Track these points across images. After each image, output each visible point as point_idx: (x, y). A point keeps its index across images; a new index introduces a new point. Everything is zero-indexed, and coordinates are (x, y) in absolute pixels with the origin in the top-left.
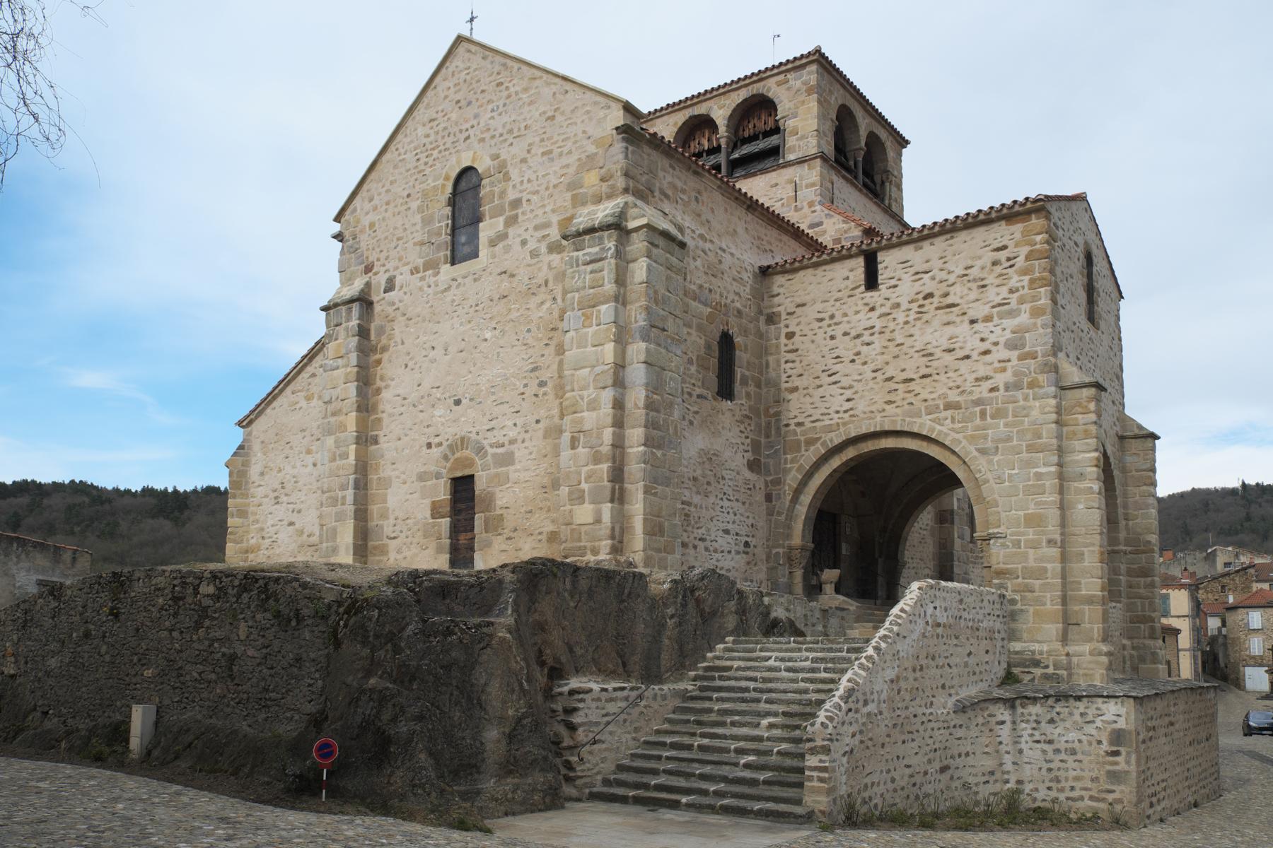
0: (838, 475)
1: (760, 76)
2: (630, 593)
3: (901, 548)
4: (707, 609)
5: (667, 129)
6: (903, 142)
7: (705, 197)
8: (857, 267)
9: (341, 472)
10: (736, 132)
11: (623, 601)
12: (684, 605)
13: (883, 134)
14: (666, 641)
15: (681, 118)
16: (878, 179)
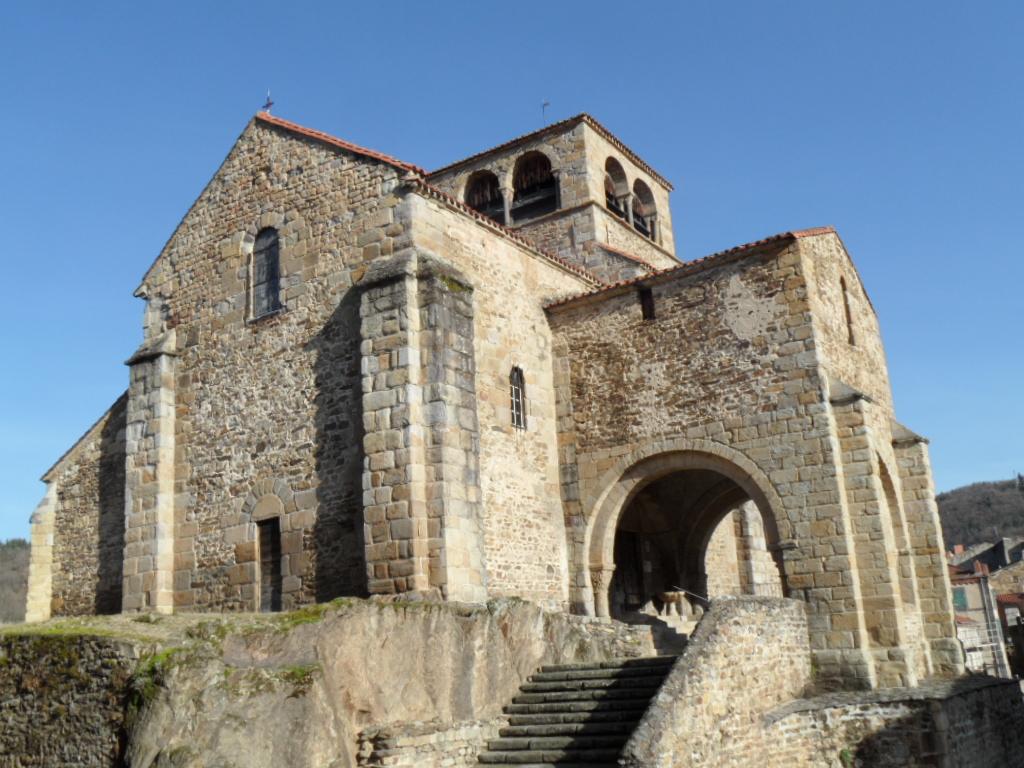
1: (536, 137)
2: (436, 628)
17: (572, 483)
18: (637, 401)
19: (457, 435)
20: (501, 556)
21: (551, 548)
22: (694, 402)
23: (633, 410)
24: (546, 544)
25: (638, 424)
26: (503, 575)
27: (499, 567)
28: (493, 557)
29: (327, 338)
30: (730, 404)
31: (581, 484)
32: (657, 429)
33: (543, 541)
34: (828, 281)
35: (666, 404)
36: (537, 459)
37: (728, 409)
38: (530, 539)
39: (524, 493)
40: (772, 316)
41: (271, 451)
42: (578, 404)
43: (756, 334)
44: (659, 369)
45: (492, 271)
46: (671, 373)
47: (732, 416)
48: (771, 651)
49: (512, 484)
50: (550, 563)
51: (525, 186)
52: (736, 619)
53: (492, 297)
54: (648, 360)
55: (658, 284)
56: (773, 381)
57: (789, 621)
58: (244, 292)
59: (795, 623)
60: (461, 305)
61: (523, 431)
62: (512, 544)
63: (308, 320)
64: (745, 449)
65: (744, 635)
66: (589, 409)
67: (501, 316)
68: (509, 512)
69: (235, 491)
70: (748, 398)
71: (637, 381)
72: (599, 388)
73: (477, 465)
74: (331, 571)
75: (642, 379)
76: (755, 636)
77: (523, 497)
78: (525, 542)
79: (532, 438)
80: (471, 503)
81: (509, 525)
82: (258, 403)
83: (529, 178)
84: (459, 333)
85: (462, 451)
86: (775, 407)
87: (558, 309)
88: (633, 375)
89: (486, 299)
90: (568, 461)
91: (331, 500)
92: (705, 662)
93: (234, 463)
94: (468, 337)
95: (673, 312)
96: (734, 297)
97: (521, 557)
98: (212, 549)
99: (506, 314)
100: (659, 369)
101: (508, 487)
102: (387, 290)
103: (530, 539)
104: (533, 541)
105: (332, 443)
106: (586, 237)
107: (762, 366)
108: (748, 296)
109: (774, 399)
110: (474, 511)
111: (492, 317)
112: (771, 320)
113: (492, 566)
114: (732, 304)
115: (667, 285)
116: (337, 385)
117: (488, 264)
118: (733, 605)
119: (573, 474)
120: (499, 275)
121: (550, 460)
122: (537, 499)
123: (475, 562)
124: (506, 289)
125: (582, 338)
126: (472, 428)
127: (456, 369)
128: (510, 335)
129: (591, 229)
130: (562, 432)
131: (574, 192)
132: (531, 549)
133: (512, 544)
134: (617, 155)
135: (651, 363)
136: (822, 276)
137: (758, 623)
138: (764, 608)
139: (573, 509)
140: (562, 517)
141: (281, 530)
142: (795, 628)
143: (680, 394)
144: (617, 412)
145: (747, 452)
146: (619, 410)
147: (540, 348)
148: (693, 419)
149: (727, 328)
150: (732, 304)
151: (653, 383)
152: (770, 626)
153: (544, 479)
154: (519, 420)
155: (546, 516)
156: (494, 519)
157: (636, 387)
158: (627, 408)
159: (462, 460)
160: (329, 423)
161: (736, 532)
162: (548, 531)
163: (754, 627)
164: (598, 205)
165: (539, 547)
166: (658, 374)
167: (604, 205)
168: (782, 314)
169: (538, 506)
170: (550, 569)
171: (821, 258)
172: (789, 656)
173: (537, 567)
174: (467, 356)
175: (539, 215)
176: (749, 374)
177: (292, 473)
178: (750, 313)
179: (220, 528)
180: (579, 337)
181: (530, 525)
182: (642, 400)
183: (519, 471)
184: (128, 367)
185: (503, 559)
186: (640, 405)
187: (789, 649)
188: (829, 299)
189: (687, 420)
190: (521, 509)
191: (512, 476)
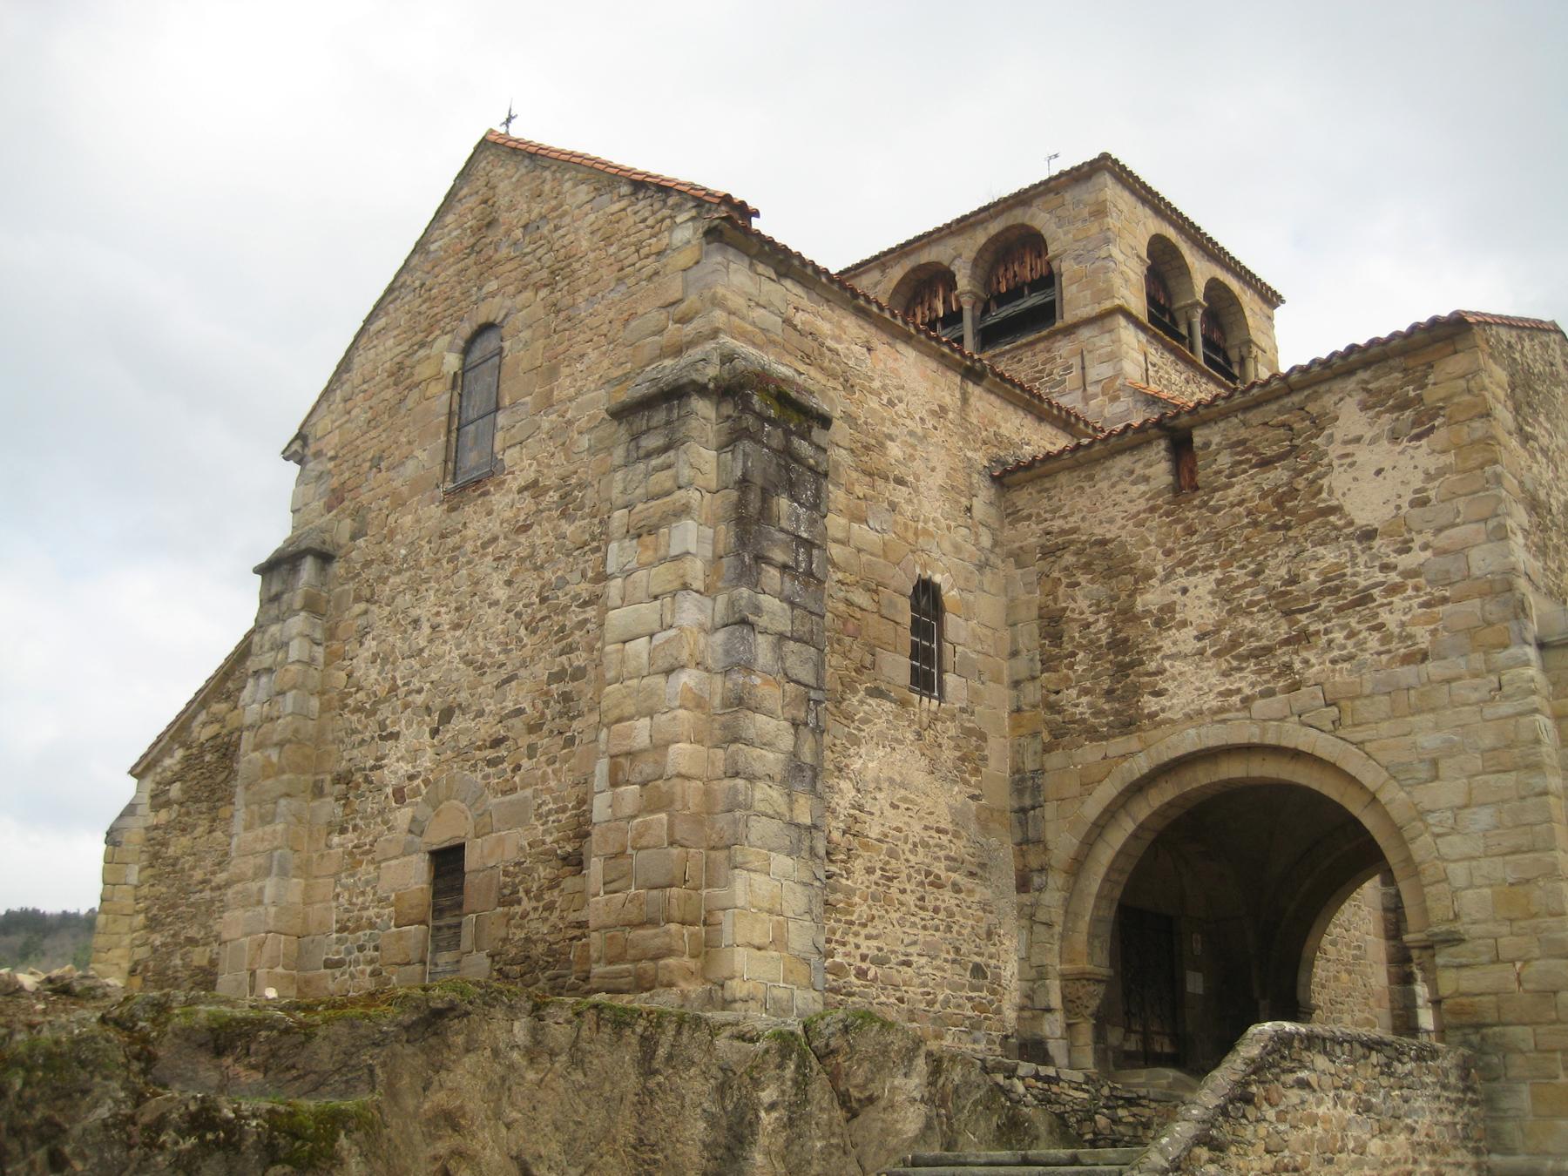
0: (1149, 837)
1: (1022, 199)
2: (670, 1057)
3: (1302, 978)
4: (855, 1093)
5: (880, 287)
6: (1271, 299)
7: (732, 266)
8: (1157, 466)
9: (260, 847)
10: (987, 285)
11: (656, 1072)
12: (801, 1083)
13: (1234, 285)
14: (759, 1158)
15: (897, 273)
16: (1234, 355)
17: (1033, 808)
18: (1159, 649)
19: (778, 693)
20: (868, 937)
21: (982, 932)
22: (1268, 650)
23: (1152, 666)
24: (970, 922)
25: (1158, 694)
26: (871, 975)
27: (864, 958)
28: (851, 939)
29: (564, 515)
30: (1336, 653)
31: (1050, 810)
32: (1196, 700)
33: (966, 917)
34: (1542, 418)
35: (1216, 654)
36: (963, 759)
37: (1334, 662)
38: (936, 910)
39: (931, 821)
40: (1422, 476)
41: (459, 722)
42: (1052, 658)
43: (1389, 511)
44: (1203, 585)
45: (885, 398)
46: (1225, 593)
47: (1342, 676)
48: (1388, 1149)
49: (905, 799)
50: (977, 959)
51: (1003, 289)
52: (1303, 1074)
53: (882, 445)
54: (1180, 570)
55: (1205, 423)
56: (1422, 605)
57: (1438, 1090)
58: (443, 439)
59: (1453, 1095)
60: (803, 447)
61: (935, 702)
62: (895, 916)
63: (535, 483)
64: (1362, 742)
65: (1321, 1111)
66: (1071, 666)
67: (900, 481)
68: (892, 854)
69: (400, 795)
70: (1373, 641)
71: (1161, 610)
72: (1088, 626)
73: (818, 754)
74: (541, 948)
75: (1169, 608)
76: (1350, 1113)
77: (926, 828)
78: (922, 914)
79: (953, 718)
80: (798, 825)
81: (890, 879)
82: (448, 636)
83: (1010, 275)
84: (793, 498)
85: (787, 724)
86: (1424, 656)
87: (1021, 475)
88: (1151, 598)
89: (867, 448)
90: (1030, 765)
91: (549, 812)
92: (1211, 1161)
93: (402, 744)
94: (815, 507)
95: (1232, 475)
96: (1346, 443)
97: (915, 943)
98: (361, 899)
99: (911, 479)
100: (1203, 585)
101: (894, 806)
102: (660, 416)
103: (936, 910)
104: (942, 915)
105: (558, 707)
106: (1106, 371)
107: (1401, 574)
108: (1373, 441)
109: (1424, 640)
110: (807, 843)
111: (879, 483)
112: (1419, 485)
113: (847, 955)
114: (1346, 455)
115: (1222, 425)
116: (574, 598)
117: (876, 384)
118: (1296, 1043)
119: (1037, 789)
120: (900, 407)
121: (992, 763)
122: (956, 835)
123: (801, 937)
124: (912, 433)
125: (1063, 532)
126: (811, 681)
127: (784, 567)
128: (915, 519)
129: (1114, 357)
130: (1019, 710)
131: (1088, 293)
132: (937, 930)
133: (895, 916)
134: (1171, 233)
135: (1187, 574)
136: (1529, 405)
137: (1359, 1088)
138: (1374, 1058)
139: (1034, 862)
140: (1013, 875)
141: (466, 869)
142: (1452, 1107)
143: (1240, 633)
144: (1122, 670)
145: (1368, 747)
146: (1124, 660)
147: (981, 549)
148: (1267, 682)
149: (1334, 503)
150: (1346, 455)
151: (1191, 616)
152: (1387, 1095)
153: (973, 797)
154: (925, 679)
155: (975, 869)
156: (858, 865)
157: (1159, 623)
158: (1142, 663)
159: (787, 741)
160: (556, 669)
161: (1386, 931)
162: (977, 898)
163: (1350, 1096)
164: (1129, 316)
165: (955, 928)
166: (1198, 600)
167: (1144, 318)
168: (1441, 472)
169: (959, 848)
170: (978, 971)
171: (1528, 371)
172: (1432, 1164)
173: (947, 966)
174: (809, 544)
175: (1022, 335)
176: (1376, 592)
177: (491, 763)
178: (1379, 472)
179: (372, 861)
180: (1056, 529)
181: (938, 884)
182: (1168, 647)
183: (919, 778)
184: (259, 577)
185: (874, 943)
186: (1165, 657)
187: (1433, 1149)
188: (1544, 452)
189: (1253, 685)
190: (920, 849)
191: (903, 786)
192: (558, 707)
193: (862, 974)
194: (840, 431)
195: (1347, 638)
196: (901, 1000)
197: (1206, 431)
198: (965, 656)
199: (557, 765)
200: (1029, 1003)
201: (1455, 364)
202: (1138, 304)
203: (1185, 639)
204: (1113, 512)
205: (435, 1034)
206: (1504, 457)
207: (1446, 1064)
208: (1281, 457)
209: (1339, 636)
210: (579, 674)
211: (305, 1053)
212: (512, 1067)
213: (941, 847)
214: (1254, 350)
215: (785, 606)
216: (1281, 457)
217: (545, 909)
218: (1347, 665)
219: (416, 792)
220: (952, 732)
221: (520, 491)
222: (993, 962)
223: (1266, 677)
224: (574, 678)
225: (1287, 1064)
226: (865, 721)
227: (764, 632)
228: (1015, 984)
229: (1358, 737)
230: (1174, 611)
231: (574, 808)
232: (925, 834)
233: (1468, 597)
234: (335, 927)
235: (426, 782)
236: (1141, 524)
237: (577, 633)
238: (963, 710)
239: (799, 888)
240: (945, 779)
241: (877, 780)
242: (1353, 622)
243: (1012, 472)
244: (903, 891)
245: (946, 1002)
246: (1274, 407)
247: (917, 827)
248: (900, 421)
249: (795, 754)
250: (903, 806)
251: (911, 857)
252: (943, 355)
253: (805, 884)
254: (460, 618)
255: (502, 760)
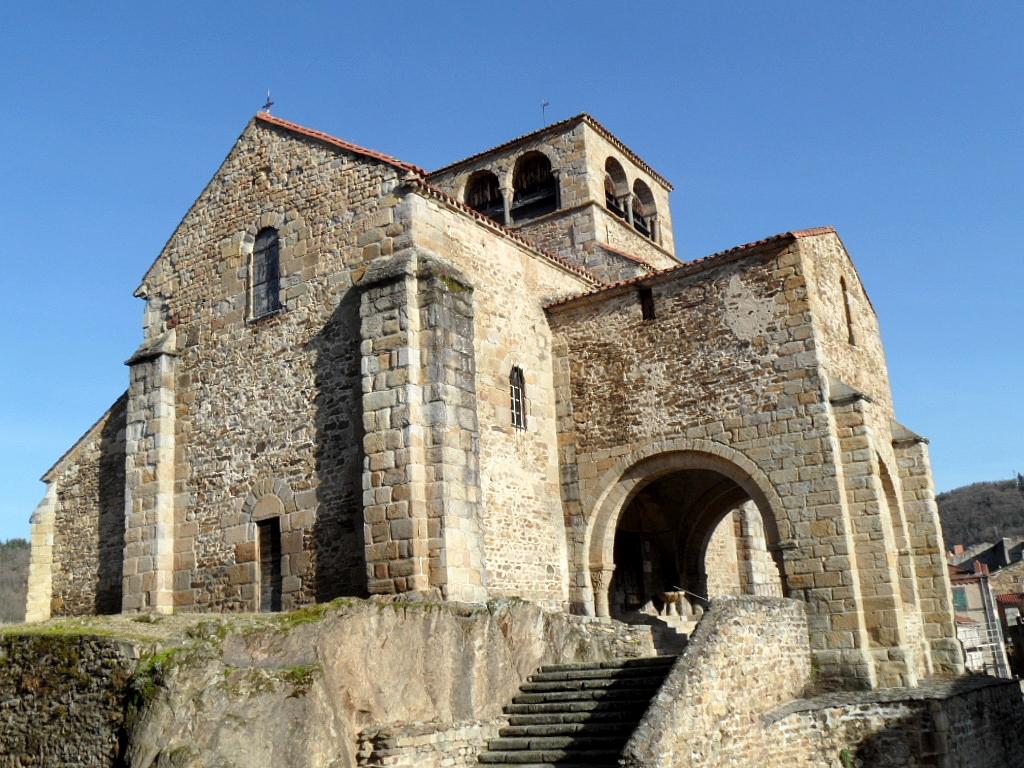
1: (536, 137)
17: (572, 483)
18: (637, 401)
20: (501, 556)
25: (638, 424)
26: (503, 576)
27: (499, 567)
28: (493, 557)
29: (327, 338)
32: (657, 429)
34: (828, 282)
36: (537, 459)
37: (728, 409)
38: (530, 539)
41: (271, 451)
44: (659, 369)
45: (492, 271)
46: (671, 373)
47: (732, 417)
50: (550, 563)
52: (736, 619)
53: (492, 297)
55: (658, 284)
59: (795, 623)
60: (461, 305)
61: (523, 431)
62: (512, 544)
66: (590, 409)
67: (501, 316)
68: (509, 512)
70: (748, 398)
73: (477, 464)
74: (331, 571)
76: (755, 635)
80: (471, 503)
81: (508, 525)
83: (529, 178)
84: (459, 333)
85: (462, 451)
86: (775, 407)
87: (559, 309)
88: (633, 375)
89: (486, 299)
91: (331, 499)
92: (704, 663)
96: (734, 297)
97: (521, 557)
99: (506, 314)
100: (659, 369)
101: (508, 487)
102: (387, 290)
103: (530, 539)
104: (533, 541)
105: (332, 444)
107: (762, 366)
109: (774, 399)
110: (475, 512)
111: (492, 317)
113: (492, 566)
114: (734, 304)
116: (337, 385)
117: (487, 265)
119: (573, 474)
120: (499, 275)
122: (537, 499)
124: (506, 289)
129: (591, 229)
132: (530, 549)
133: (512, 544)
134: (618, 155)
137: (758, 623)
138: (764, 608)
144: (617, 412)
147: (540, 348)
148: (693, 419)
151: (653, 383)
153: (543, 479)
154: (519, 420)
156: (494, 519)
164: (597, 205)
166: (658, 374)
167: (604, 206)
168: (782, 314)
169: (538, 506)
170: (550, 569)
171: (821, 258)
172: (789, 656)
174: (467, 356)
182: (642, 400)
183: (518, 471)
185: (503, 559)
187: (788, 649)
188: (829, 299)
189: (687, 420)
190: (521, 508)
191: (511, 476)
192: (332, 444)
193: (499, 575)
194: (476, 294)
195: (735, 397)
196: (517, 587)
197: (659, 288)
198: (536, 406)
199: (334, 474)
200: (574, 584)
201: (786, 259)
202: (602, 199)
203: (649, 396)
204: (610, 328)
205: (339, 627)
206: (812, 307)
207: (792, 608)
208: (698, 303)
209: (731, 396)
210: (344, 425)
211: (285, 643)
212: (371, 640)
213: (529, 506)
214: (659, 217)
215: (458, 390)
216: (698, 303)
217: (332, 550)
218: (735, 411)
219: (245, 489)
220: (531, 446)
221: (298, 324)
222: (556, 564)
223: (693, 416)
224: (341, 427)
225: (729, 614)
226: (492, 444)
227: (450, 404)
228: (567, 574)
229: (743, 447)
230: (644, 382)
231: (347, 496)
232: (523, 500)
233: (795, 378)
234: (197, 565)
235: (252, 484)
236: (625, 336)
237: (341, 403)
238: (536, 434)
239: (473, 535)
240: (530, 471)
241: (500, 474)
242: (738, 389)
243: (555, 305)
244: (515, 531)
245: (537, 585)
246: (695, 277)
247: (519, 496)
248: (500, 283)
249: (467, 466)
250: (512, 487)
251: (518, 513)
252: (518, 245)
253: (475, 533)
254: (265, 393)
255: (299, 471)
